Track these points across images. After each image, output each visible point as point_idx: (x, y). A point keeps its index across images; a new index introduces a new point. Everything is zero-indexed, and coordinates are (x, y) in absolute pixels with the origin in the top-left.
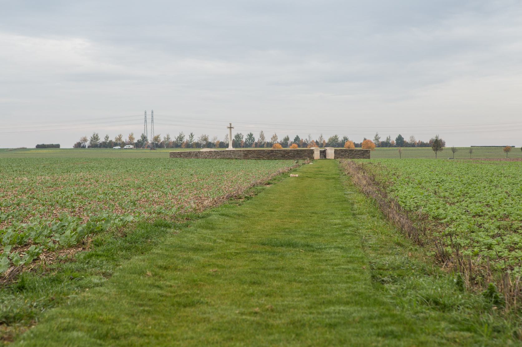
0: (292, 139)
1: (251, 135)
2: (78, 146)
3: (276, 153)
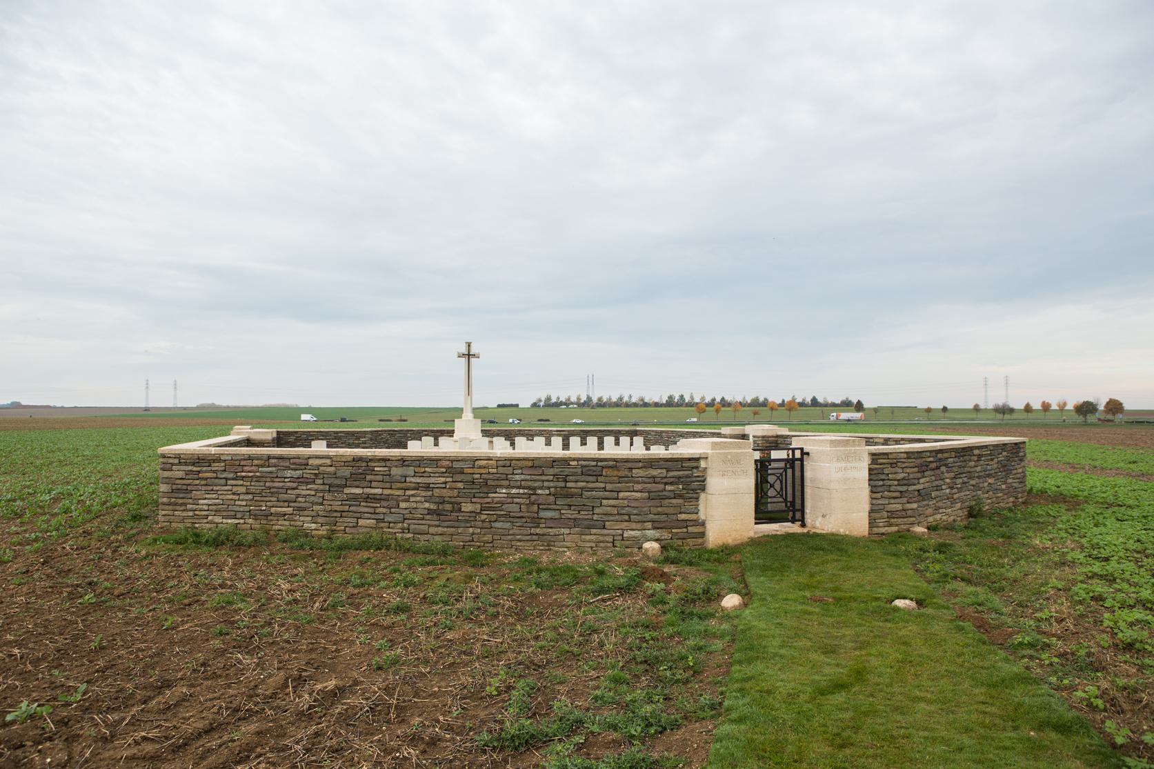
0: (718, 400)
1: (682, 396)
2: (535, 405)
3: (389, 481)
